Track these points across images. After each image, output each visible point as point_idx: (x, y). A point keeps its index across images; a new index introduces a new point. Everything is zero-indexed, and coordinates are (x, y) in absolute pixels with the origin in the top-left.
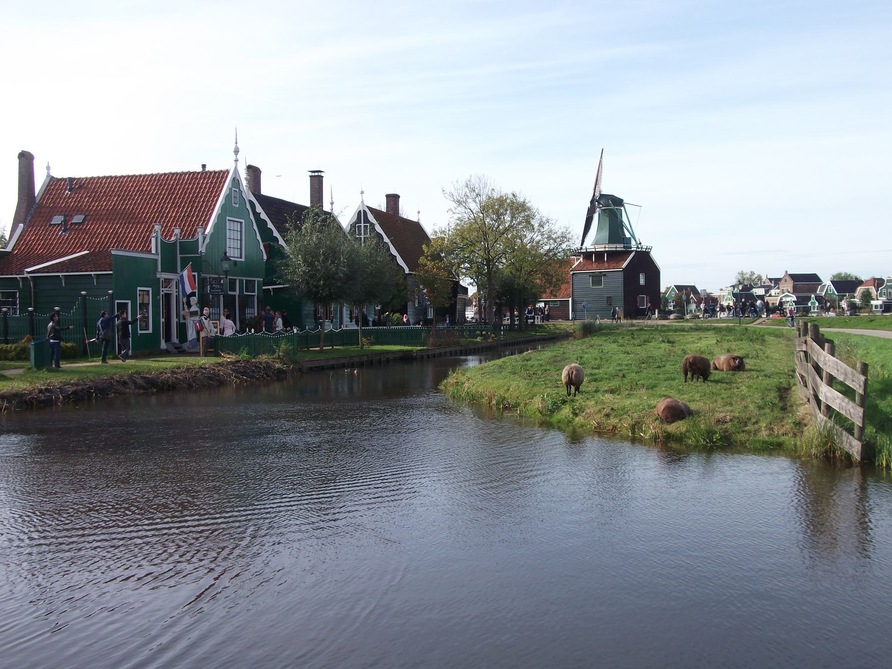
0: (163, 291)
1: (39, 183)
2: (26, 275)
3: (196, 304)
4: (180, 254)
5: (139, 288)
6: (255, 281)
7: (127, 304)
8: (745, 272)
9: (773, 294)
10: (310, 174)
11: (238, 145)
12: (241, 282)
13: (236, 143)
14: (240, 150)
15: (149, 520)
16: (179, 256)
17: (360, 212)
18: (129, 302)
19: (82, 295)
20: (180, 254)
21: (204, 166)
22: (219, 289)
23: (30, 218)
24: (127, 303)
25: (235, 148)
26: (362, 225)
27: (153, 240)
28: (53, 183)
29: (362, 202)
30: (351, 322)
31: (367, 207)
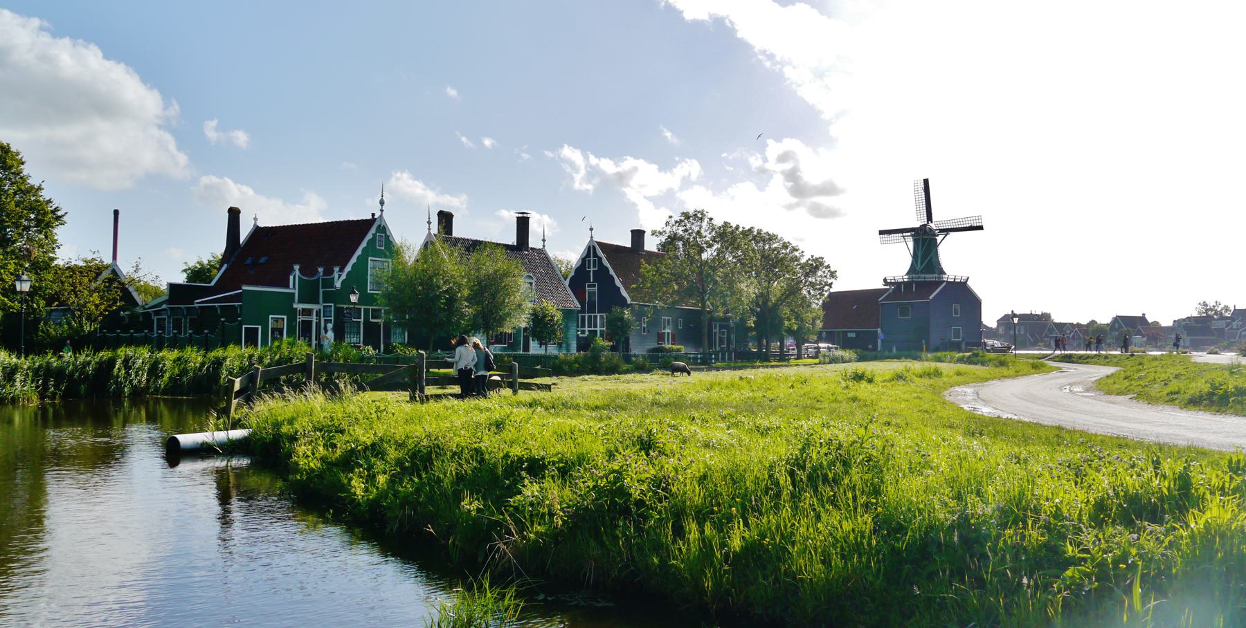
0: (300, 318)
1: (244, 233)
2: (196, 305)
5: (271, 316)
7: (258, 328)
8: (1207, 303)
9: (1235, 327)
10: (518, 215)
11: (384, 198)
15: (868, 546)
16: (321, 290)
17: (590, 247)
18: (260, 327)
19: (222, 321)
21: (373, 215)
24: (258, 328)
26: (592, 259)
27: (291, 278)
28: (258, 232)
29: (592, 237)
30: (541, 347)
31: (597, 242)
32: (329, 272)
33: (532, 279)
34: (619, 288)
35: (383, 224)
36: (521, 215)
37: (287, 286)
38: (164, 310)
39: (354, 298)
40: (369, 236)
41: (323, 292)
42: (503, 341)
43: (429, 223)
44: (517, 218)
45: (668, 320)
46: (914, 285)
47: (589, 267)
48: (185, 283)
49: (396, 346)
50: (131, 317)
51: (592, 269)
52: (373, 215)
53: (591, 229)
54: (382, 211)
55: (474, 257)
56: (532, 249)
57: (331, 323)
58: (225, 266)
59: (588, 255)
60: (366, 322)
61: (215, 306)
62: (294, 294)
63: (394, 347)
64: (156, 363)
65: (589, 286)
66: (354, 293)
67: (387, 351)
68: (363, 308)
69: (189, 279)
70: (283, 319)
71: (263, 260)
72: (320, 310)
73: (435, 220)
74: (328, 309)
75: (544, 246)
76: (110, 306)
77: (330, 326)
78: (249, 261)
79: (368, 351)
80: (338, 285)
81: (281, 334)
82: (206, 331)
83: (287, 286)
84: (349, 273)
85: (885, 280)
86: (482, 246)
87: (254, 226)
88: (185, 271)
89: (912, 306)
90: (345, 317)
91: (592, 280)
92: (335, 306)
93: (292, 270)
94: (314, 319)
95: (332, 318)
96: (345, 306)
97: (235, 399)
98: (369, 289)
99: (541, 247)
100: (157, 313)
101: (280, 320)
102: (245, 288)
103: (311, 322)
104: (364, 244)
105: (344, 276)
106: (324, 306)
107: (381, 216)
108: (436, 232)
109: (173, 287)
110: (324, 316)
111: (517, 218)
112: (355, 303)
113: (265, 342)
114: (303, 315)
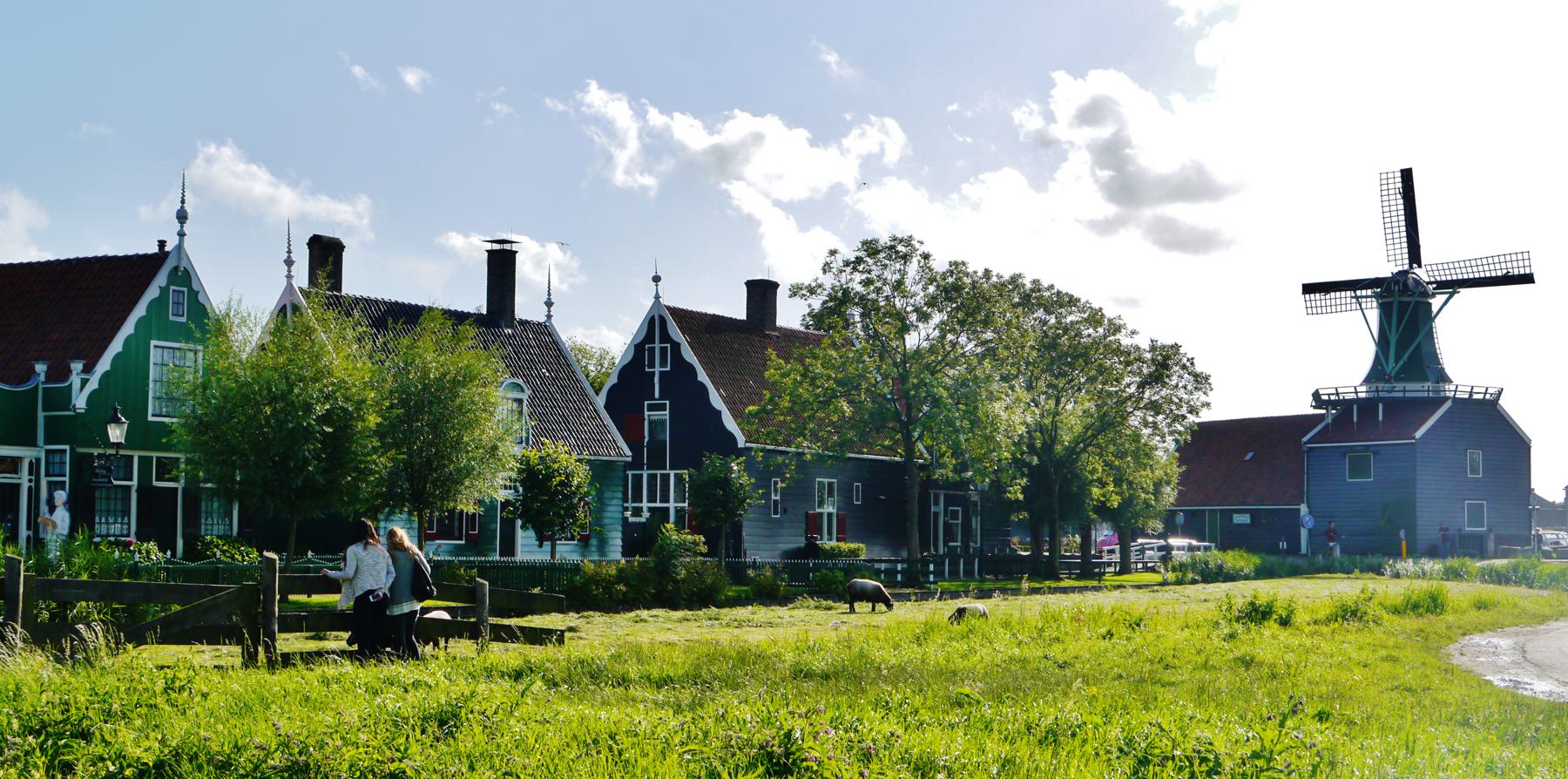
3: (64, 504)
4: (44, 410)
6: (132, 457)
10: (489, 246)
12: (144, 462)
16: (41, 415)
20: (44, 410)
21: (162, 244)
22: (104, 477)
25: (178, 211)
26: (657, 346)
29: (657, 297)
31: (668, 308)
32: (59, 373)
33: (523, 391)
34: (719, 413)
35: (184, 264)
36: (496, 247)
39: (116, 434)
40: (152, 293)
41: (45, 417)
42: (456, 533)
43: (289, 263)
44: (490, 252)
45: (830, 484)
46: (1381, 406)
47: (652, 365)
49: (212, 542)
51: (657, 369)
52: (162, 244)
53: (657, 279)
54: (181, 235)
56: (523, 323)
57: (63, 489)
59: (649, 337)
60: (145, 489)
63: (208, 545)
65: (651, 408)
66: (117, 421)
72: (38, 460)
74: (57, 458)
75: (549, 317)
77: (61, 496)
80: (80, 402)
85: (1316, 395)
89: (1375, 453)
90: (96, 476)
91: (657, 395)
92: (72, 450)
94: (24, 479)
95: (67, 479)
96: (96, 452)
98: (150, 411)
99: (542, 319)
104: (140, 310)
105: (94, 384)
106: (48, 452)
107: (180, 247)
111: (490, 252)
112: (118, 445)
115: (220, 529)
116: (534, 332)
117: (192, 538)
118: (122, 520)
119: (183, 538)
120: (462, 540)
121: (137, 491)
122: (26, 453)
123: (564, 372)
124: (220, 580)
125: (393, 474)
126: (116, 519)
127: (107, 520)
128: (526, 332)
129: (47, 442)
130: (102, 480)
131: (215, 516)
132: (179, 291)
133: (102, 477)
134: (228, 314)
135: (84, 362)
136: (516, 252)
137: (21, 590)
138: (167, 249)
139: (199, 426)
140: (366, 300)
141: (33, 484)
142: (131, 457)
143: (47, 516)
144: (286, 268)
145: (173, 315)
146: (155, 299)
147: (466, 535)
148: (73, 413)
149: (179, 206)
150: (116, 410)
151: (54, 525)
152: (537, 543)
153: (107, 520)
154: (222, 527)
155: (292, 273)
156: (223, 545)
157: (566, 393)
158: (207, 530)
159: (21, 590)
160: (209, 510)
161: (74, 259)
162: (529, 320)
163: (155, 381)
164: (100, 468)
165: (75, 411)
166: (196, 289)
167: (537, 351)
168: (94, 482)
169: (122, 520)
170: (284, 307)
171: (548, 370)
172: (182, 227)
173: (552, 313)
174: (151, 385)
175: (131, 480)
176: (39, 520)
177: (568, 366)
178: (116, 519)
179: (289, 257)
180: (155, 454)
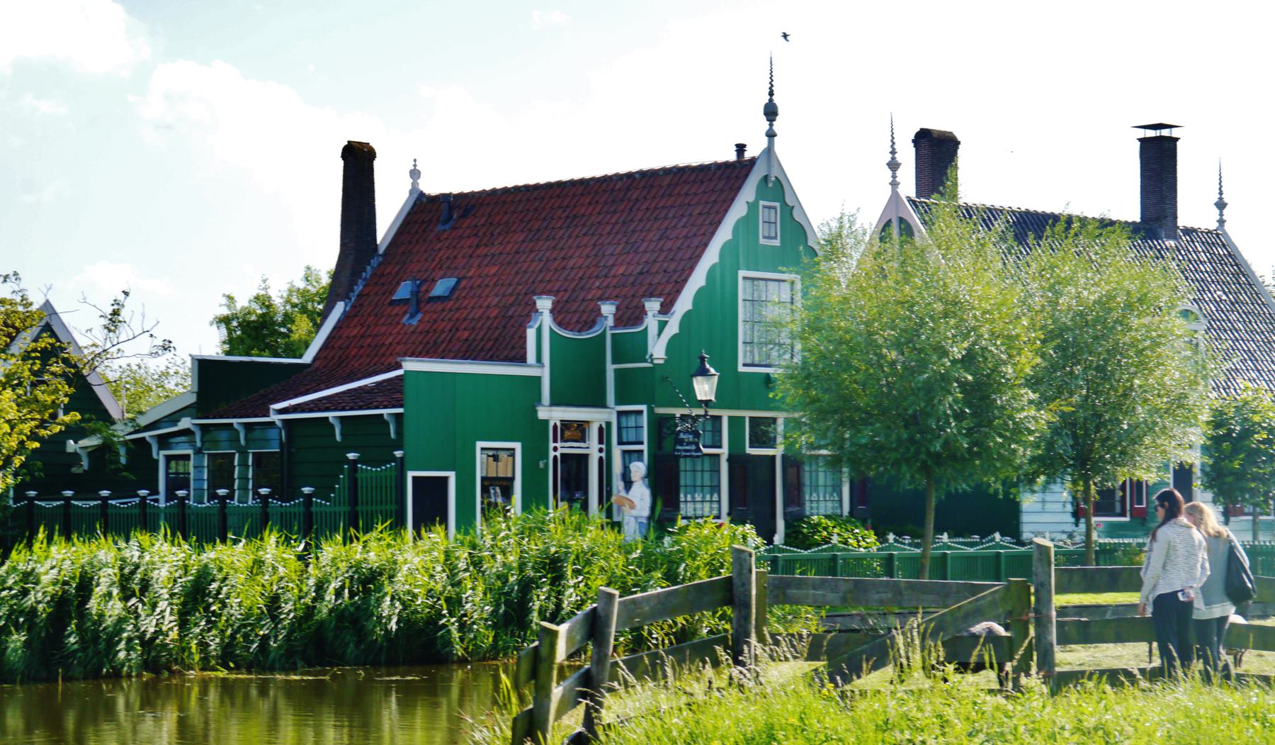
2: (274, 418)
3: (643, 479)
4: (614, 362)
7: (445, 479)
12: (735, 423)
13: (771, 94)
14: (780, 111)
16: (610, 368)
18: (452, 476)
19: (348, 461)
20: (614, 362)
21: (741, 148)
23: (361, 287)
24: (415, 478)
27: (531, 334)
32: (631, 315)
35: (774, 173)
36: (1151, 133)
37: (521, 359)
38: (187, 432)
39: (704, 389)
40: (738, 210)
41: (616, 371)
43: (894, 165)
44: (1143, 141)
48: (223, 357)
49: (819, 524)
50: (97, 454)
52: (741, 148)
54: (771, 135)
55: (1040, 255)
56: (1189, 231)
57: (640, 459)
58: (339, 308)
61: (144, 438)
62: (537, 380)
63: (815, 527)
64: (204, 577)
66: (703, 372)
67: (794, 537)
68: (725, 414)
69: (233, 344)
70: (511, 452)
71: (442, 287)
72: (609, 424)
73: (907, 156)
74: (632, 421)
75: (1221, 222)
76: (43, 424)
77: (639, 469)
78: (404, 290)
79: (744, 538)
80: (658, 350)
81: (507, 493)
82: (307, 490)
83: (521, 359)
84: (687, 317)
86: (1060, 227)
87: (411, 192)
88: (225, 321)
90: (681, 442)
92: (651, 410)
93: (532, 309)
94: (593, 449)
95: (644, 447)
96: (678, 412)
97: (558, 684)
98: (741, 361)
99: (1213, 225)
100: (164, 441)
101: (503, 455)
102: (411, 365)
103: (584, 459)
104: (724, 234)
105: (673, 328)
106: (620, 414)
107: (769, 151)
108: (913, 195)
109: (205, 367)
110: (620, 443)
111: (1143, 141)
112: (707, 403)
113: (465, 521)
114: (564, 440)
115: (829, 507)
116: (1203, 243)
117: (795, 521)
118: (711, 497)
119: (785, 520)
120: (1125, 516)
121: (728, 460)
122: (594, 417)
123: (1246, 293)
124: (839, 573)
125: (1056, 431)
126: (704, 497)
127: (693, 497)
128: (1193, 242)
129: (619, 401)
130: (688, 448)
131: (821, 490)
132: (769, 208)
133: (689, 444)
134: (840, 235)
135: (662, 300)
136: (1177, 139)
137: (754, 592)
138: (748, 155)
139: (805, 377)
140: (988, 209)
141: (603, 455)
142: (719, 418)
143: (623, 493)
144: (890, 173)
145: (764, 237)
146: (743, 218)
147: (1131, 510)
148: (650, 365)
149: (766, 99)
150: (703, 359)
151: (632, 506)
152: (1073, 520)
153: (693, 497)
154: (830, 504)
155: (898, 179)
156: (834, 527)
157: (1250, 322)
158: (812, 508)
159: (754, 592)
160: (814, 484)
161: (637, 172)
162: (1196, 227)
163: (745, 321)
164: (684, 433)
165: (652, 362)
166: (790, 204)
167: (1209, 267)
168: (679, 450)
169: (711, 497)
170: (888, 224)
171: (1225, 293)
172: (771, 125)
173: (1224, 218)
174: (741, 327)
175: (720, 447)
176: (613, 499)
177: (1250, 285)
178: (704, 497)
179: (893, 158)
180: (747, 414)
